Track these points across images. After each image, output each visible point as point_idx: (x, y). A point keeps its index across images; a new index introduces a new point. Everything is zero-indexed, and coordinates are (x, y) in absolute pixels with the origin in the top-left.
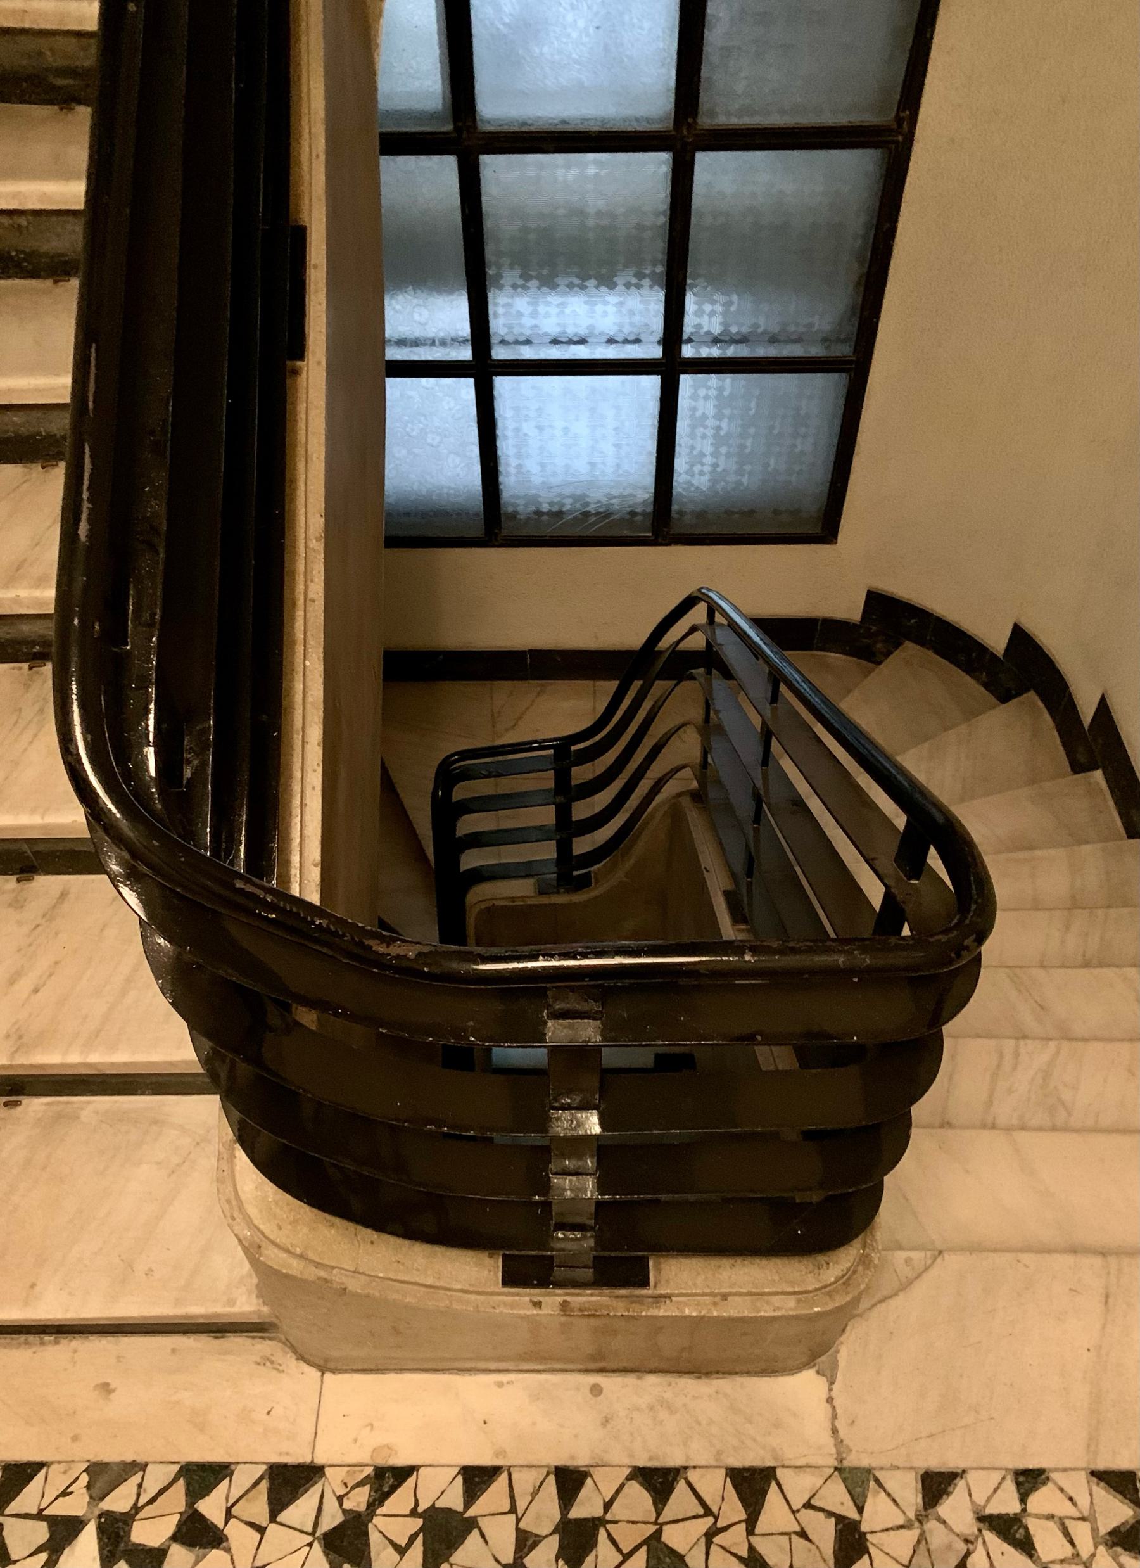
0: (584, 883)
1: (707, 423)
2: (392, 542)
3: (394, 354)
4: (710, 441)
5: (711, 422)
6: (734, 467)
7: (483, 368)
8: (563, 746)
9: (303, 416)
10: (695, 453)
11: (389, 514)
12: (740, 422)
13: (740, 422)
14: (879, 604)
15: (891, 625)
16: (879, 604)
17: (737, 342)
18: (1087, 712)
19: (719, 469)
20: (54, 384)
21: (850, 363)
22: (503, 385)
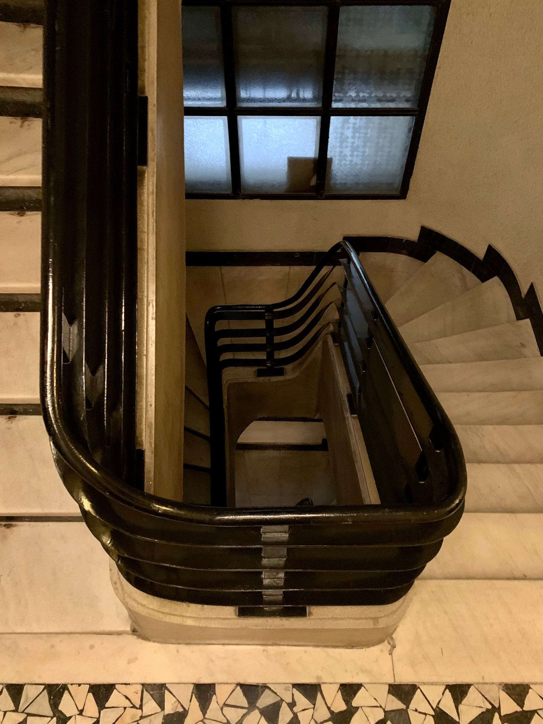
0: (281, 373)
1: (348, 140)
2: (190, 196)
3: (187, 104)
7: (232, 111)
8: (269, 308)
10: (342, 155)
11: (186, 184)
12: (361, 158)
13: (361, 158)
14: (425, 232)
15: (429, 244)
16: (425, 232)
18: (524, 290)
20: (34, 78)
21: (418, 112)
22: (247, 124)
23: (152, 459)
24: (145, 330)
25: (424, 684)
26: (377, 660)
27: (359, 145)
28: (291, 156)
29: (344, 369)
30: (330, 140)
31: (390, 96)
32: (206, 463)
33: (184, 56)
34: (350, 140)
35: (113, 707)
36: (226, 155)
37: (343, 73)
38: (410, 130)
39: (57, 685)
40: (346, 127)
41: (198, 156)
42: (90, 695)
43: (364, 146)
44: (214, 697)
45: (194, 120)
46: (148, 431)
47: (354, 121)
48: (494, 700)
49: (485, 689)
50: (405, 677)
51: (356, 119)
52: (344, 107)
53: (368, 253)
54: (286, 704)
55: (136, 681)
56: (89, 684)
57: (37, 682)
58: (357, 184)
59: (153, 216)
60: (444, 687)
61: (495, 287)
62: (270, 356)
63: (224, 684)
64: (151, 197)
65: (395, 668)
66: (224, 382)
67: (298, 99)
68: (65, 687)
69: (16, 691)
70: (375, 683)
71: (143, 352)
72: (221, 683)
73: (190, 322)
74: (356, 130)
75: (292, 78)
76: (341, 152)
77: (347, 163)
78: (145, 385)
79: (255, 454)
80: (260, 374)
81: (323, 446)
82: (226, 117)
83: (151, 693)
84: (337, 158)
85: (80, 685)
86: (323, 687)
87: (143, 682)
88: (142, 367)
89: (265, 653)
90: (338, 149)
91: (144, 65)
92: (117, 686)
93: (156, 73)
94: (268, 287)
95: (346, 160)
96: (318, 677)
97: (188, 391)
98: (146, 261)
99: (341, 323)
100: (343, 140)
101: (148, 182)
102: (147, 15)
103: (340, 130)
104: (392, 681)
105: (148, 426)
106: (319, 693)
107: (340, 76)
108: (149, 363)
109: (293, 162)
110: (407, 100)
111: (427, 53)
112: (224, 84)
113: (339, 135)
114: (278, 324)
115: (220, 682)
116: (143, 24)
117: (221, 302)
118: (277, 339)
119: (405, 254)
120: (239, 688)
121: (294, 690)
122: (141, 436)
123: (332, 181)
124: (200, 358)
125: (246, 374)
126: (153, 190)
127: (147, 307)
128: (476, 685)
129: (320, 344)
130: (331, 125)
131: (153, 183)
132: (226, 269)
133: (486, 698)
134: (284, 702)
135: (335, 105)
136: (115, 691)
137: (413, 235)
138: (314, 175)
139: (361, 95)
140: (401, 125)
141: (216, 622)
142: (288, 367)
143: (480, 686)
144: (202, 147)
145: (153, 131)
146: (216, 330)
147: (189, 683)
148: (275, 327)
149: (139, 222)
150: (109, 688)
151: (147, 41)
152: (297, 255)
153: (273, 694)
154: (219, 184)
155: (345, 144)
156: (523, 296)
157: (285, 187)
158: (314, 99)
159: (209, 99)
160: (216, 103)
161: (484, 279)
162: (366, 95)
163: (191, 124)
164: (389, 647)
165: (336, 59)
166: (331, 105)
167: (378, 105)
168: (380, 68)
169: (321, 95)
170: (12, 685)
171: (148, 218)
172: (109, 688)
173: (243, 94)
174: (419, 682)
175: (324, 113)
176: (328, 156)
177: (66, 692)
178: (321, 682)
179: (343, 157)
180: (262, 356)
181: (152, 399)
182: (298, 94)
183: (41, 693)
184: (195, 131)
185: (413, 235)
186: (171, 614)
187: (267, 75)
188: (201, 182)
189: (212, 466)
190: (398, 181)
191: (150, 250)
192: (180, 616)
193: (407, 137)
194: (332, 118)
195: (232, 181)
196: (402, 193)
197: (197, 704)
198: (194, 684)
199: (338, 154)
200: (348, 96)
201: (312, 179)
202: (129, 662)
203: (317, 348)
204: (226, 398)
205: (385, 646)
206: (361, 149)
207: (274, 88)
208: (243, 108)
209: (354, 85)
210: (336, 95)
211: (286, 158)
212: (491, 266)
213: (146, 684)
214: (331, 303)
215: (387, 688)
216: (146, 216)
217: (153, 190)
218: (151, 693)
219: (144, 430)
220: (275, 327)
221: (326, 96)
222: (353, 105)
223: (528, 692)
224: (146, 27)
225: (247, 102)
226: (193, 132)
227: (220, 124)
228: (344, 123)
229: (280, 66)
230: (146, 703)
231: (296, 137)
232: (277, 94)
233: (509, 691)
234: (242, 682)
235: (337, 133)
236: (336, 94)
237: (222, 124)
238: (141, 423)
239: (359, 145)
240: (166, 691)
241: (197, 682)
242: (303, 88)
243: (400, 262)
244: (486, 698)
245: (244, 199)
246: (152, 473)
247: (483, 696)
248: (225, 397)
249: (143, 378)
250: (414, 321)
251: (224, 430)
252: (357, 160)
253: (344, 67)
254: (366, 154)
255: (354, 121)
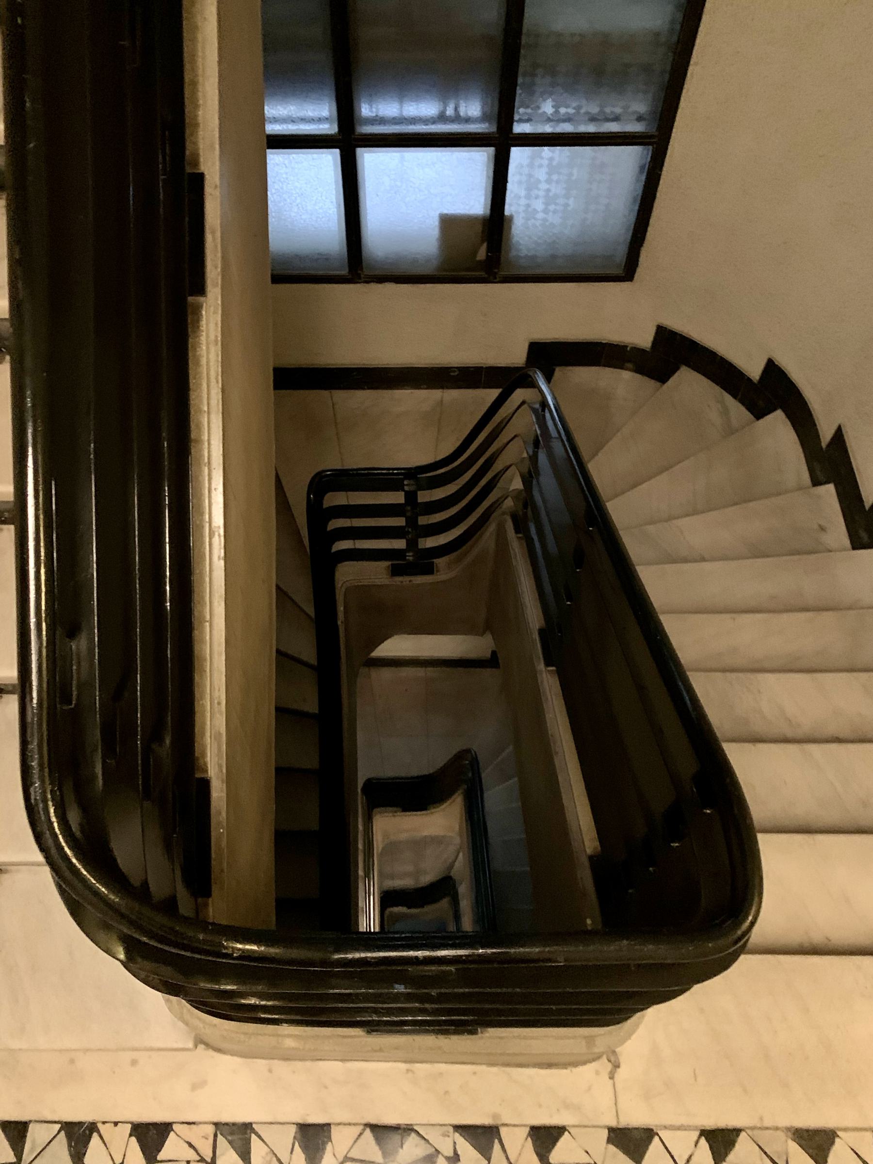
0: (429, 570)
1: (540, 186)
3: (272, 128)
4: (544, 170)
5: (544, 186)
6: (564, 192)
7: (348, 141)
8: (412, 473)
9: (207, 579)
10: (530, 210)
12: (565, 186)
14: (664, 335)
15: (670, 354)
16: (664, 335)
17: (564, 121)
18: (826, 434)
19: (551, 194)
21: (656, 140)
22: (371, 160)
23: (222, 791)
24: (207, 579)
25: (665, 1127)
26: (590, 1089)
27: (559, 194)
28: (445, 212)
29: (533, 582)
30: (509, 186)
31: (612, 112)
32: (312, 706)
33: (265, 50)
34: (544, 186)
35: (170, 1161)
36: (338, 211)
37: (533, 75)
38: (642, 168)
39: (80, 1124)
40: (536, 164)
41: (293, 214)
42: (133, 1139)
43: (567, 196)
44: (329, 1147)
45: (286, 156)
46: (215, 746)
47: (551, 154)
48: (779, 1157)
49: (764, 1138)
50: (635, 1117)
51: (553, 152)
52: (532, 132)
53: (570, 368)
54: (444, 1160)
55: (207, 1120)
56: (132, 1123)
57: (49, 1118)
58: (554, 257)
59: (217, 382)
60: (698, 1133)
61: (777, 428)
62: (412, 544)
63: (345, 1124)
64: (213, 350)
65: (620, 1100)
66: (339, 584)
67: (457, 118)
68: (93, 1127)
69: (17, 1131)
70: (585, 1126)
71: (205, 617)
72: (339, 1124)
73: (284, 483)
74: (552, 169)
75: (447, 81)
76: (528, 206)
77: (538, 223)
78: (208, 671)
79: (386, 674)
80: (396, 571)
81: (492, 662)
82: (337, 151)
83: (230, 1138)
84: (522, 215)
85: (116, 1124)
86: (503, 1131)
87: (215, 1120)
88: (203, 641)
89: (410, 1075)
90: (523, 202)
91: (196, 116)
92: (174, 1127)
93: (217, 130)
94: (408, 433)
95: (535, 219)
96: (495, 1116)
97: (281, 592)
98: (206, 460)
99: (526, 499)
100: (531, 185)
101: (207, 325)
102: (200, 24)
103: (526, 170)
104: (613, 1123)
105: (215, 739)
106: (496, 1141)
107: (528, 80)
108: (215, 632)
109: (448, 223)
110: (640, 119)
111: (675, 38)
112: (333, 88)
113: (524, 178)
114: (424, 497)
115: (338, 1121)
116: (194, 40)
117: (332, 462)
118: (423, 520)
119: (630, 370)
120: (368, 1130)
121: (457, 1135)
122: (204, 755)
123: (513, 253)
124: (301, 541)
125: (376, 573)
126: (216, 336)
127: (210, 539)
128: (748, 1131)
129: (491, 528)
130: (511, 161)
131: (216, 324)
132: (340, 396)
133: (765, 1153)
134: (440, 1156)
135: (519, 128)
136: (172, 1133)
137: (644, 339)
138: (483, 242)
139: (563, 110)
140: (627, 161)
141: (331, 1041)
142: (440, 562)
143: (756, 1132)
144: (298, 201)
145: (213, 233)
146: (325, 506)
147: (288, 1123)
148: (419, 501)
149: (193, 395)
150: (162, 1130)
151: (200, 72)
152: (454, 372)
153: (423, 1142)
154: (327, 259)
155: (535, 192)
156: (824, 445)
157: (435, 263)
158: (484, 118)
159: (311, 120)
160: (321, 126)
161: (759, 413)
162: (571, 111)
163: (280, 164)
164: (609, 1066)
165: (522, 51)
166: (511, 129)
167: (591, 128)
168: (595, 64)
169: (496, 109)
170: (10, 1122)
171: (208, 386)
172: (162, 1130)
173: (365, 110)
174: (656, 1126)
175: (501, 141)
176: (507, 213)
177: (95, 1135)
178: (499, 1123)
179: (530, 213)
180: (400, 544)
181: (221, 694)
182: (456, 109)
183: (54, 1137)
184: (286, 173)
185: (644, 339)
186: (258, 1034)
187: (405, 79)
188: (297, 256)
189: (322, 793)
190: (621, 253)
191: (212, 442)
192: (273, 1035)
193: (638, 180)
194: (514, 150)
195: (348, 251)
196: (628, 271)
197: (303, 1156)
198: (297, 1124)
199: (522, 209)
200: (540, 113)
201: (480, 250)
202: (194, 1087)
203: (488, 534)
204: (342, 608)
205: (603, 1065)
206: (561, 201)
207: (416, 101)
208: (365, 135)
209: (551, 94)
210: (520, 112)
211: (438, 213)
212: (771, 391)
213: (221, 1123)
214: (510, 466)
215: (605, 1133)
216: (205, 385)
217: (216, 336)
218: (230, 1138)
219: (209, 746)
220: (419, 501)
221: (504, 113)
222: (548, 129)
223: (833, 1143)
224: (200, 46)
225: (373, 125)
226: (284, 176)
227: (326, 164)
228: (532, 158)
229: (429, 62)
230: (223, 1154)
231: (453, 183)
232: (421, 110)
233: (803, 1142)
234: (373, 1121)
235: (521, 174)
236: (521, 110)
237: (331, 163)
238: (203, 734)
239: (559, 194)
240: (253, 1136)
241: (301, 1122)
242: (466, 99)
243: (623, 382)
244: (765, 1153)
245: (367, 282)
246: (224, 814)
247: (760, 1147)
248: (341, 608)
249: (205, 660)
250: (644, 485)
251: (340, 658)
252: (555, 219)
253: (535, 66)
254: (569, 209)
255: (551, 154)
